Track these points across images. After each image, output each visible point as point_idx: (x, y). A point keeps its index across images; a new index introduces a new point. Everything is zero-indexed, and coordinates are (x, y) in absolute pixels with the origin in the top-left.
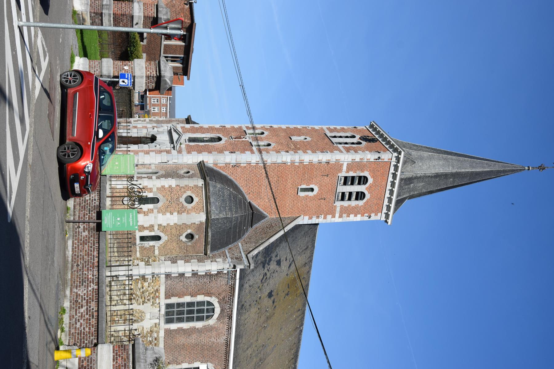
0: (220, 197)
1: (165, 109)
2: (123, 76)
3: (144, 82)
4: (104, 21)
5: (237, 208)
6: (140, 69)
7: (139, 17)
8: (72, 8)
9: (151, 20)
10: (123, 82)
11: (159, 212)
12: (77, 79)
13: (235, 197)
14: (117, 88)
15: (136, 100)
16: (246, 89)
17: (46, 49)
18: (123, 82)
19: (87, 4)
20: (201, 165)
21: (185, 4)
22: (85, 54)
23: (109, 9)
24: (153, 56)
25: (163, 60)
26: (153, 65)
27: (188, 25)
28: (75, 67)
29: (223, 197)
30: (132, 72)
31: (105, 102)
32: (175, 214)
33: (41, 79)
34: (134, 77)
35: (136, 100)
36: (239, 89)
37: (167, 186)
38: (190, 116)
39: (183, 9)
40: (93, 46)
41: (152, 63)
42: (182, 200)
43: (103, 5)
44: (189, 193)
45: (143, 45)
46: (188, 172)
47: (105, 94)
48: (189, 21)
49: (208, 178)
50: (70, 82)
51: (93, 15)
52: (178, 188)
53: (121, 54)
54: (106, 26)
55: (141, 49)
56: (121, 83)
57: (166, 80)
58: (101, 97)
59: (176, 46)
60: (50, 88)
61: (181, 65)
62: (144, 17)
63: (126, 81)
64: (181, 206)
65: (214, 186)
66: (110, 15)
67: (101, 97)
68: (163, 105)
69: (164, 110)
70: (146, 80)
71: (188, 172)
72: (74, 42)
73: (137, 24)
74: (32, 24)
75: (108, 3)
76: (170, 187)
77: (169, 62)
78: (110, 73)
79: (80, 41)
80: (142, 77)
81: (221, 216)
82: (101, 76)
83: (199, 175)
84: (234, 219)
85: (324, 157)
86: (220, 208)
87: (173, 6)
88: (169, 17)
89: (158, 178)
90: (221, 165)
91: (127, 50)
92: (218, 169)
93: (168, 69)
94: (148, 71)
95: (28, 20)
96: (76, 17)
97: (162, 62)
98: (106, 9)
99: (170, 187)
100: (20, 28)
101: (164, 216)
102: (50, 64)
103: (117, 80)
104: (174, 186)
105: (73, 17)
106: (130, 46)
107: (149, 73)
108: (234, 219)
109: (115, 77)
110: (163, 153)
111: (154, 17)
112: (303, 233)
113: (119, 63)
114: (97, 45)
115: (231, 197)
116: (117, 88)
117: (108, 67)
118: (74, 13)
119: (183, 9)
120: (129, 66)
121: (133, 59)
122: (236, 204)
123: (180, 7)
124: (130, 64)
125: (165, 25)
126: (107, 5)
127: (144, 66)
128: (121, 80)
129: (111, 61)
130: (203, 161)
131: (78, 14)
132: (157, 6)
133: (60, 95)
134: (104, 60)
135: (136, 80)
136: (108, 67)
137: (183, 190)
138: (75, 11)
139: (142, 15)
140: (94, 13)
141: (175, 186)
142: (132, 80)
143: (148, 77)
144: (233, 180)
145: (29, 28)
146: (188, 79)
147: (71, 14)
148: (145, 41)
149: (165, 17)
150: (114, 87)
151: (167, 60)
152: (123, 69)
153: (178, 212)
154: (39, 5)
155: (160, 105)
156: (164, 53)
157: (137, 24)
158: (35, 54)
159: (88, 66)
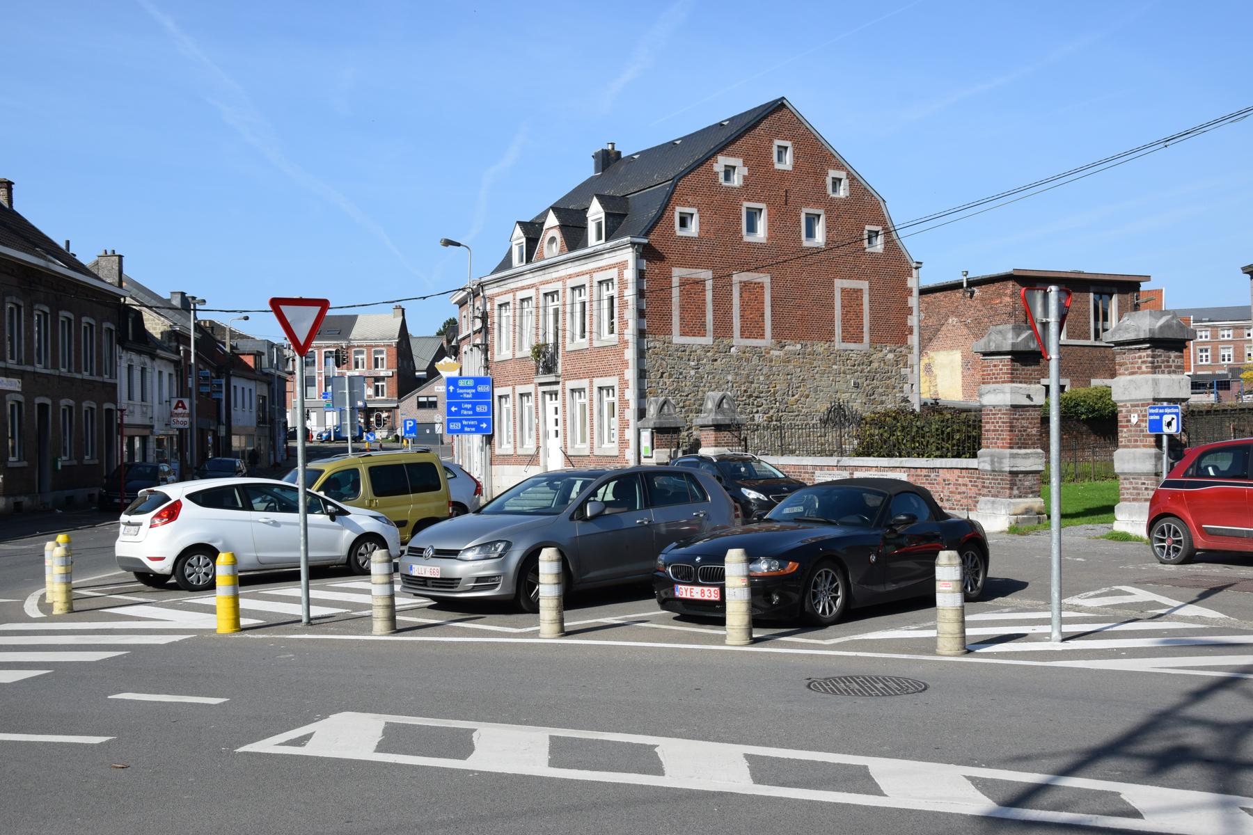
1: (1226, 333)
2: (1156, 425)
3: (1166, 376)
6: (1132, 387)
7: (1013, 392)
8: (1005, 535)
10: (1169, 424)
12: (1169, 527)
14: (1184, 438)
15: (1206, 399)
16: (1175, 132)
17: (1104, 590)
18: (1169, 424)
19: (993, 503)
21: (971, 296)
22: (1108, 510)
23: (1001, 458)
24: (1104, 361)
25: (1107, 338)
26: (1124, 357)
27: (1018, 287)
28: (1142, 531)
30: (1143, 405)
31: (1225, 465)
33: (1176, 603)
34: (1155, 400)
35: (1206, 399)
36: (1173, 148)
38: (1243, 269)
39: (982, 300)
40: (1089, 493)
41: (1118, 359)
45: (1072, 385)
47: (1203, 465)
48: (1010, 284)
50: (1179, 542)
51: (1016, 492)
53: (1095, 433)
55: (1082, 391)
56: (1173, 430)
57: (1161, 327)
58: (1212, 473)
60: (1198, 586)
61: (1115, 298)
62: (1012, 382)
63: (1166, 418)
66: (1013, 456)
67: (1212, 473)
68: (1214, 336)
69: (1227, 334)
70: (1163, 372)
72: (1082, 531)
73: (1029, 397)
74: (1056, 612)
75: (988, 459)
77: (1108, 325)
79: (1075, 520)
80: (1155, 382)
82: (1157, 474)
85: (676, 292)
87: (978, 322)
88: (1009, 326)
93: (1125, 324)
94: (1139, 368)
95: (1047, 622)
96: (1022, 527)
97: (1117, 339)
98: (1000, 463)
100: (1067, 638)
102: (1138, 583)
103: (1165, 439)
105: (1024, 534)
106: (1076, 413)
107: (1144, 367)
109: (1158, 443)
110: (1153, 461)
111: (1012, 360)
112: (914, 340)
113: (1123, 434)
116: (1184, 438)
117: (1135, 459)
118: (1013, 530)
119: (982, 300)
120: (1129, 412)
121: (1114, 405)
123: (980, 307)
124: (1124, 410)
125: (1038, 327)
126: (992, 462)
128: (1166, 430)
129: (1119, 454)
132: (985, 354)
133: (1210, 565)
134: (1118, 467)
135: (1162, 396)
136: (1135, 459)
139: (1008, 386)
140: (1011, 489)
142: (1165, 404)
143: (1155, 369)
145: (1063, 621)
146: (1147, 278)
147: (1016, 537)
149: (1010, 335)
150: (1185, 446)
151: (1105, 330)
152: (1137, 425)
154: (1008, 599)
155: (1216, 343)
156: (1088, 338)
157: (1029, 397)
158: (1119, 612)
159: (1136, 504)
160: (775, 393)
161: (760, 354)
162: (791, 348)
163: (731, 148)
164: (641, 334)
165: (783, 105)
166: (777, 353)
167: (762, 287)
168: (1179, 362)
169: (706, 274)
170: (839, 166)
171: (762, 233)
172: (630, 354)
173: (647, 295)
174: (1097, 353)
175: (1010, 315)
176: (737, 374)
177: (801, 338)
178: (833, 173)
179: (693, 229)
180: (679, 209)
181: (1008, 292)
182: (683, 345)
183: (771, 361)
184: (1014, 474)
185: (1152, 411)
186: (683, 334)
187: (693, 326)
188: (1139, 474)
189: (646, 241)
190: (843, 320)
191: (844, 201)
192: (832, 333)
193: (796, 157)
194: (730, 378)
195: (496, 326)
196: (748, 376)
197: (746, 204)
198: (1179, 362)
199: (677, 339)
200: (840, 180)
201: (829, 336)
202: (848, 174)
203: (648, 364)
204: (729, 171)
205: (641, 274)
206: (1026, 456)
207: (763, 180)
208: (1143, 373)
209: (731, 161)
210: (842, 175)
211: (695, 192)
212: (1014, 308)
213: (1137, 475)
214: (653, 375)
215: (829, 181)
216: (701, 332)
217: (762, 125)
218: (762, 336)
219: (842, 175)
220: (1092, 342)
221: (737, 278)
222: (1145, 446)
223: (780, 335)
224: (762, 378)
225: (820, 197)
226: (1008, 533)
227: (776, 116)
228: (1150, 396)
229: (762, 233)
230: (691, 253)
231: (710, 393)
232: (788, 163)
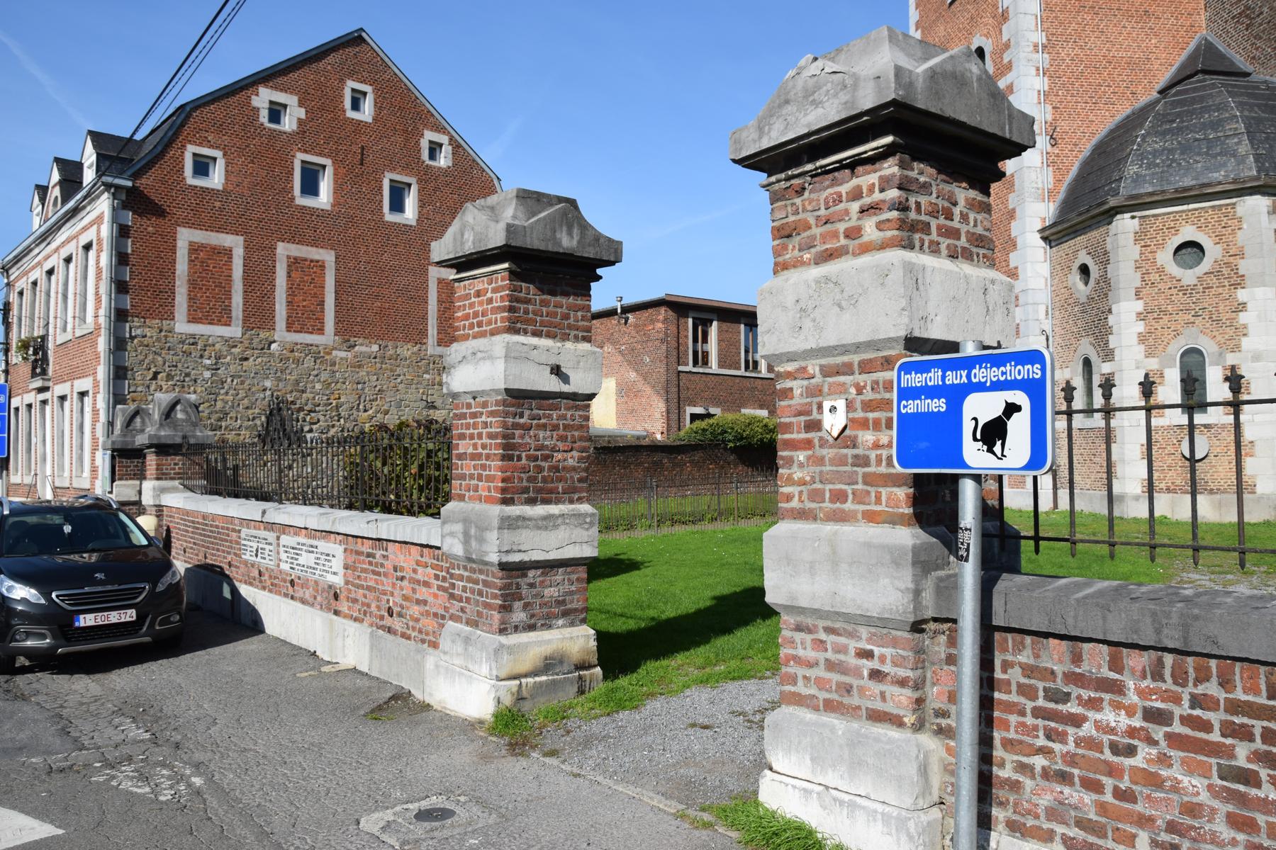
0: (1173, 160)
3: (947, 264)
4: (553, 556)
5: (1206, 109)
7: (511, 356)
9: (529, 290)
10: (993, 433)
11: (1236, 348)
13: (1164, 118)
18: (993, 433)
20: (1054, 235)
27: (670, 313)
29: (1171, 151)
30: (866, 367)
32: (1242, 295)
34: (914, 344)
37: (1140, 327)
39: (636, 326)
42: (1189, 277)
43: (470, 560)
44: (1165, 257)
46: (1084, 270)
48: (663, 310)
49: (1113, 202)
51: (519, 616)
52: (1144, 291)
54: (799, 432)
59: (720, 341)
64: (1213, 281)
65: (1134, 181)
66: (509, 524)
70: (935, 250)
71: (1084, 270)
73: (556, 371)
75: (458, 528)
76: (1141, 316)
78: (894, 556)
80: (915, 279)
81: (1244, 148)
83: (1094, 234)
84: (1246, 113)
86: (1215, 156)
89: (1108, 355)
90: (1051, 179)
91: (733, 450)
92: (1063, 188)
98: (481, 540)
99: (1141, 316)
101: (1251, 330)
104: (1139, 306)
106: (723, 441)
108: (1246, 113)
111: (513, 274)
113: (796, 469)
114: (718, 526)
115: (1169, 131)
120: (816, 392)
122: (1191, 113)
124: (797, 386)
127: (816, 272)
129: (780, 539)
130: (1041, 231)
131: (520, 698)
137: (1154, 277)
138: (497, 716)
140: (506, 609)
141: (1141, 302)
143: (910, 232)
144: (1094, 141)
148: (712, 411)
153: (1235, 286)
156: (739, 368)
157: (556, 371)
160: (337, 407)
161: (317, 355)
162: (363, 349)
163: (280, 80)
164: (120, 316)
165: (360, 37)
166: (343, 354)
167: (323, 267)
168: (977, 223)
169: (235, 243)
170: (439, 129)
171: (325, 197)
172: (102, 344)
173: (132, 260)
174: (747, 383)
175: (662, 341)
176: (279, 379)
177: (378, 337)
178: (429, 135)
179: (216, 179)
180: (191, 149)
181: (661, 317)
182: (193, 336)
183: (333, 364)
184: (513, 570)
185: (916, 380)
186: (192, 319)
187: (210, 306)
188: (848, 618)
189: (129, 184)
190: (439, 318)
191: (445, 172)
192: (424, 333)
193: (378, 106)
194: (268, 384)
195: (15, 320)
196: (297, 382)
197: (301, 156)
198: (977, 223)
199: (182, 326)
200: (441, 145)
201: (419, 337)
202: (451, 139)
203: (130, 358)
204: (276, 112)
205: (123, 232)
206: (548, 523)
207: (325, 125)
208: (866, 249)
209: (281, 97)
210: (444, 139)
211: (221, 129)
212: (666, 334)
213: (842, 622)
214: (140, 376)
215: (424, 144)
216: (224, 317)
217: (331, 59)
218: (321, 331)
219: (444, 139)
220: (742, 372)
221: (284, 250)
222: (871, 517)
223: (348, 330)
224: (318, 386)
225: (411, 162)
226: (493, 730)
227: (351, 51)
228: (896, 328)
229: (325, 197)
230: (207, 210)
231: (158, 395)
232: (367, 113)
